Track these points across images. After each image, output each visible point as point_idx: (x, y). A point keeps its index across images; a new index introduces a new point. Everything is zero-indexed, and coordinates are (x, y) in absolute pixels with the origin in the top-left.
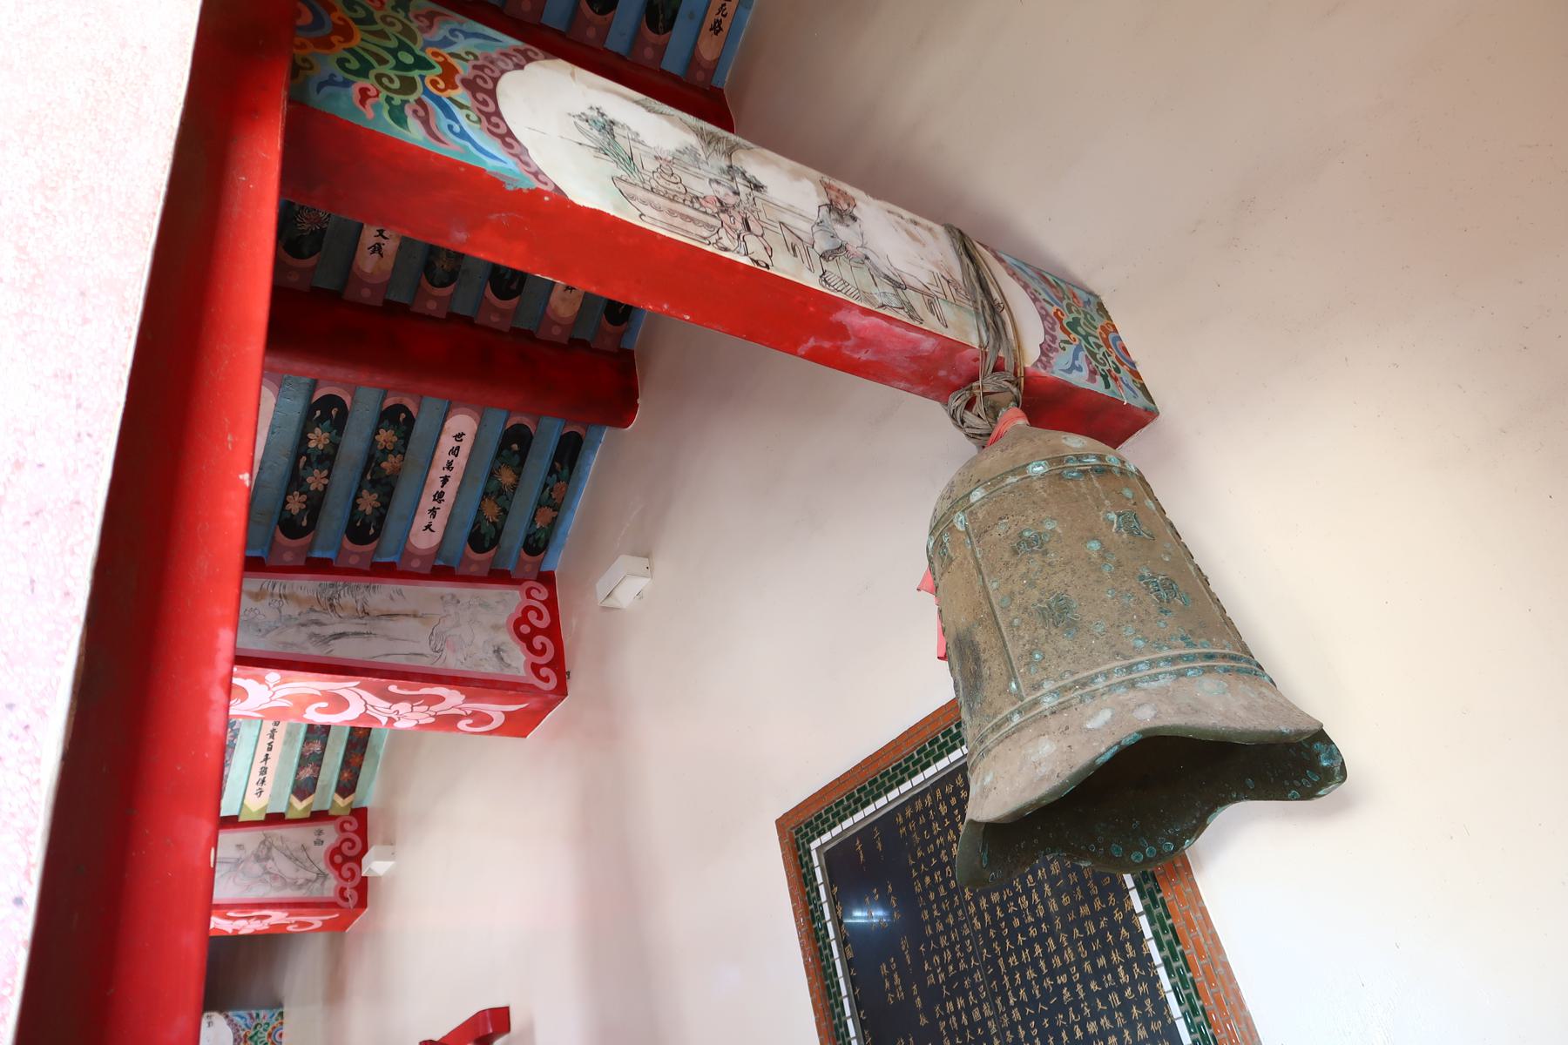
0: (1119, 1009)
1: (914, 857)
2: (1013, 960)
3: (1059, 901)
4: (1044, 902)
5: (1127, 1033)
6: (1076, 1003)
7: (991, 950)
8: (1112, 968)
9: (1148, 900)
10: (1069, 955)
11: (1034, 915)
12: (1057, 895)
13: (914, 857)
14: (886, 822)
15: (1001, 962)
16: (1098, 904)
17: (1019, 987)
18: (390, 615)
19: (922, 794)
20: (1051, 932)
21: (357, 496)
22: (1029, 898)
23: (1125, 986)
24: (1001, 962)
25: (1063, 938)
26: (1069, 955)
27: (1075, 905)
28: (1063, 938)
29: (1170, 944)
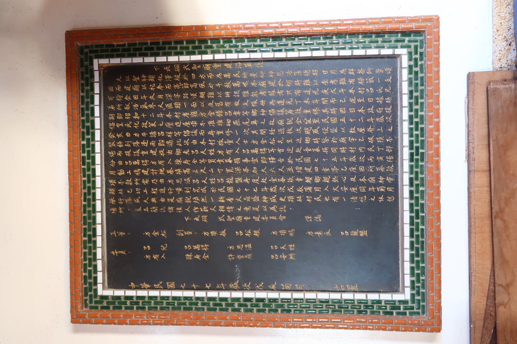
0: (250, 93)
1: (137, 206)
2: (212, 152)
3: (193, 109)
4: (190, 119)
5: (261, 93)
6: (242, 118)
7: (202, 166)
8: (233, 89)
9: (209, 51)
10: (219, 114)
11: (194, 128)
12: (190, 109)
13: (137, 206)
14: (113, 222)
15: (210, 161)
16: (202, 86)
17: (225, 153)
18: (495, 328)
19: (108, 185)
20: (206, 120)
21: (509, 300)
22: (186, 128)
23: (242, 85)
24: (210, 161)
25: (211, 114)
26: (219, 114)
27: (198, 99)
28: (211, 114)
29: (89, 194)
